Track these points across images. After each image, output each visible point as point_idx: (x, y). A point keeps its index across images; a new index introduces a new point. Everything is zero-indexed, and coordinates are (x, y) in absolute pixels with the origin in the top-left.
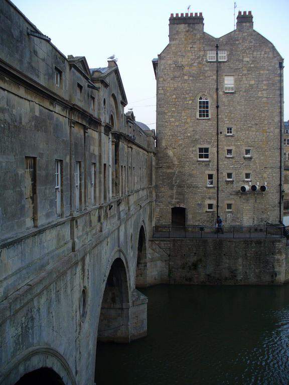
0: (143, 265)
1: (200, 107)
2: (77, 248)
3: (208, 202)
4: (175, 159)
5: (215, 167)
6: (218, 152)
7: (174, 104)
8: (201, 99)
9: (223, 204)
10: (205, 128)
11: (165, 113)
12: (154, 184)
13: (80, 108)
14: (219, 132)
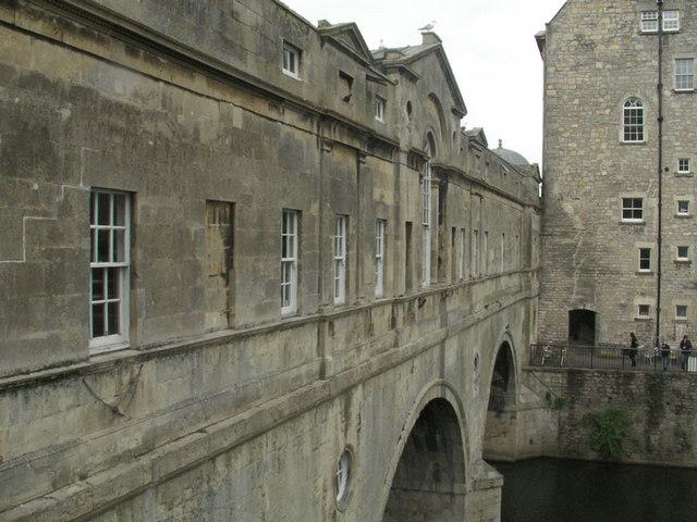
0: (509, 415)
1: (626, 121)
2: (330, 372)
3: (639, 301)
4: (577, 218)
5: (655, 234)
6: (660, 206)
7: (576, 116)
8: (627, 104)
9: (670, 307)
10: (635, 161)
11: (558, 133)
12: (535, 265)
13: (344, 118)
14: (663, 168)
